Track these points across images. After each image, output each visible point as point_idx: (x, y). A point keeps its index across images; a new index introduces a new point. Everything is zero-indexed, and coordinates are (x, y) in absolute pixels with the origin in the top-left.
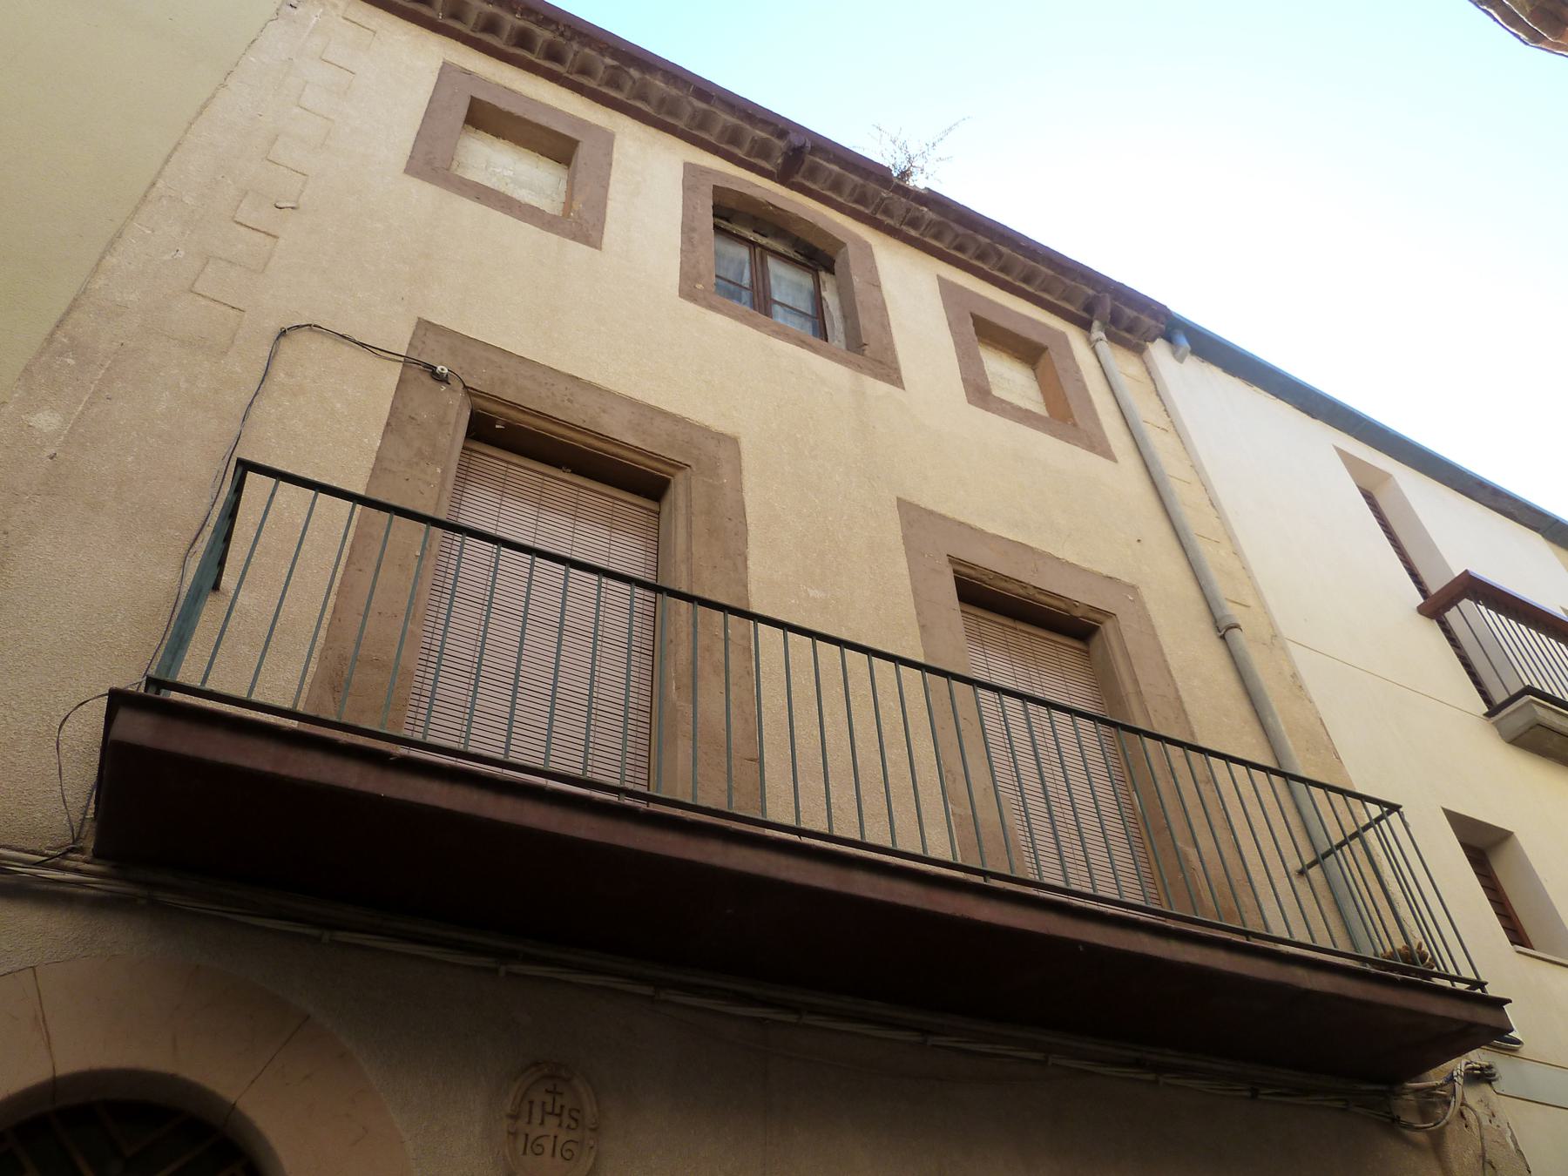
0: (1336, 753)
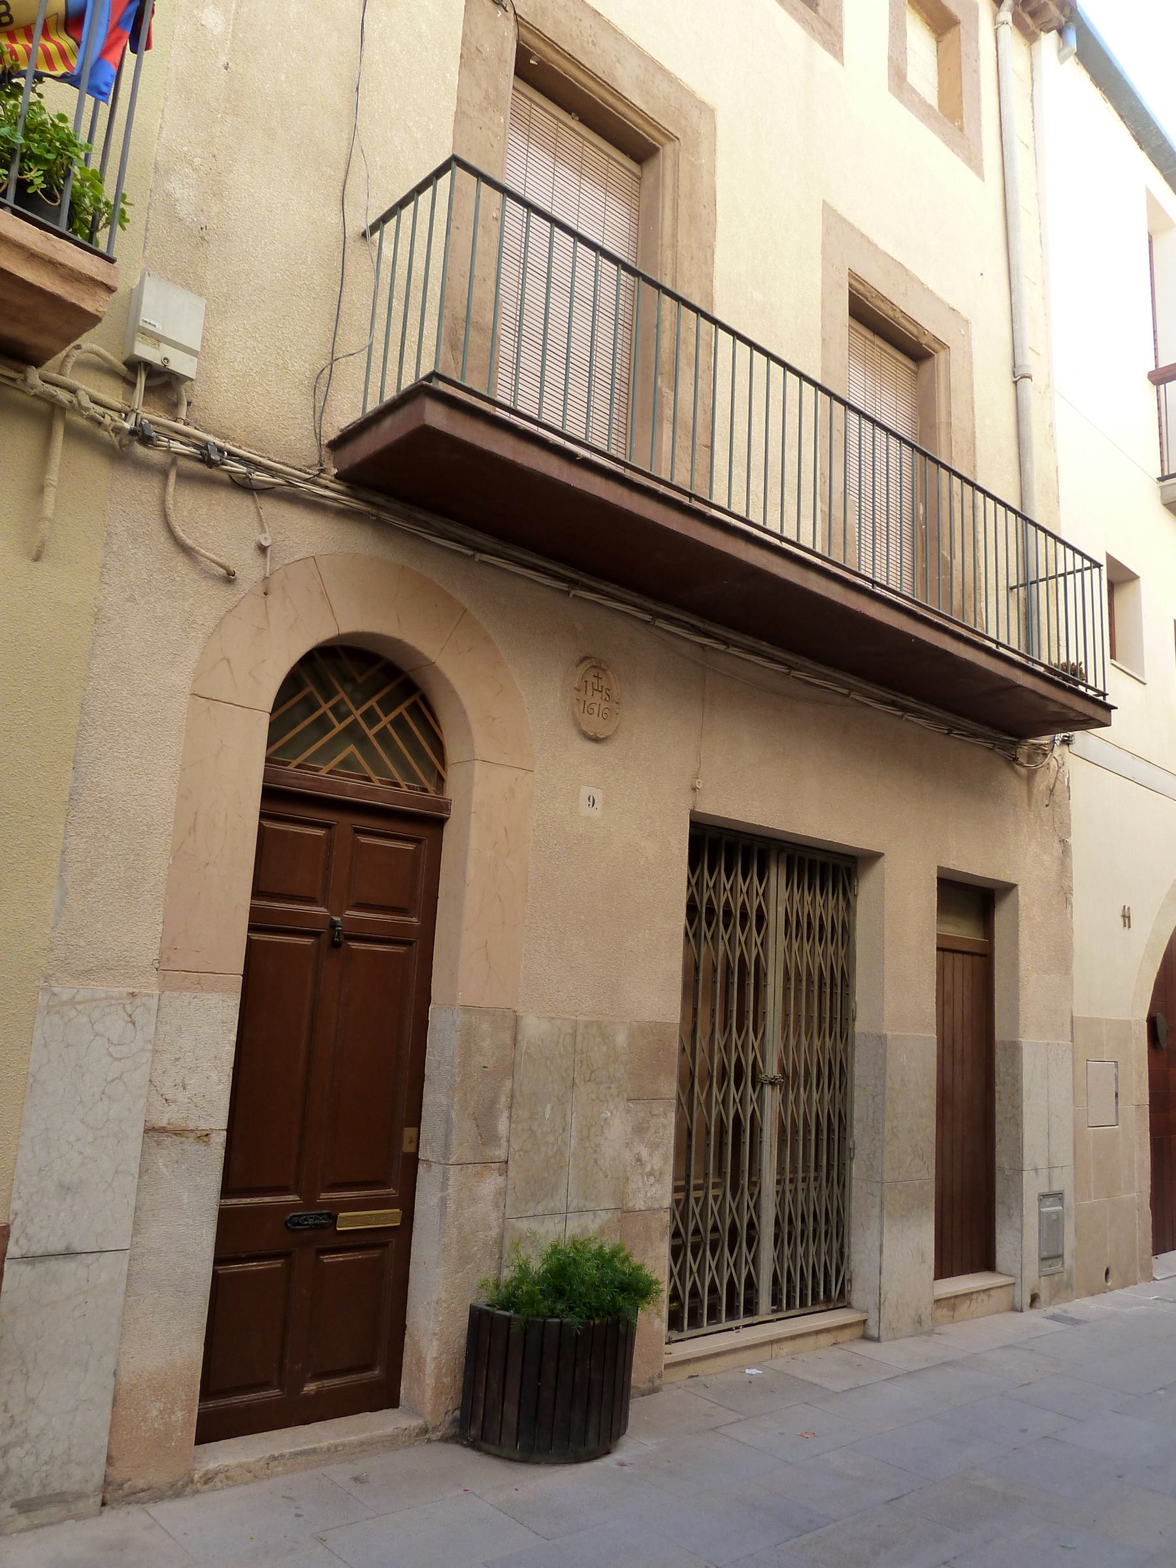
0: (1058, 497)
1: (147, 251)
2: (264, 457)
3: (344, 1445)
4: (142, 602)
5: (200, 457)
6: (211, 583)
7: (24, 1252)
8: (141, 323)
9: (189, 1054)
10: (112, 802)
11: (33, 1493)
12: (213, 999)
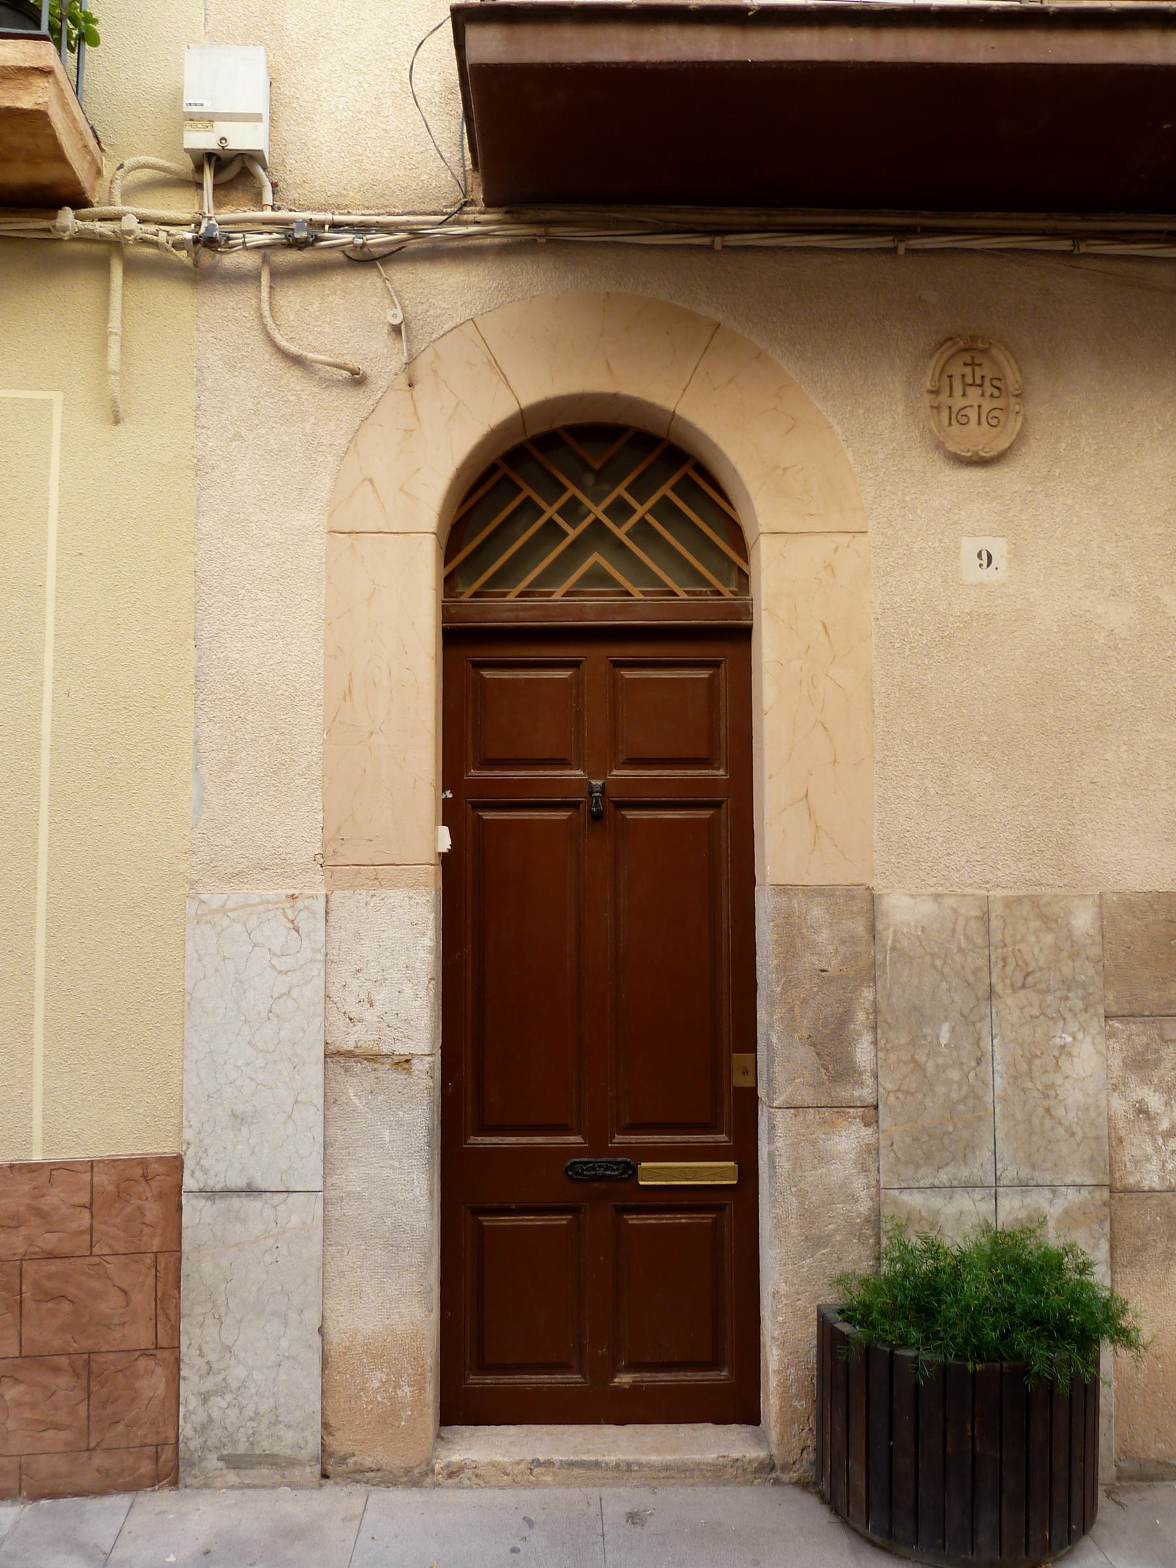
1: (210, 24)
2: (383, 214)
3: (640, 1465)
4: (251, 438)
5: (285, 241)
6: (334, 392)
7: (202, 1185)
8: (186, 109)
9: (373, 964)
10: (244, 677)
11: (242, 1448)
12: (397, 896)
